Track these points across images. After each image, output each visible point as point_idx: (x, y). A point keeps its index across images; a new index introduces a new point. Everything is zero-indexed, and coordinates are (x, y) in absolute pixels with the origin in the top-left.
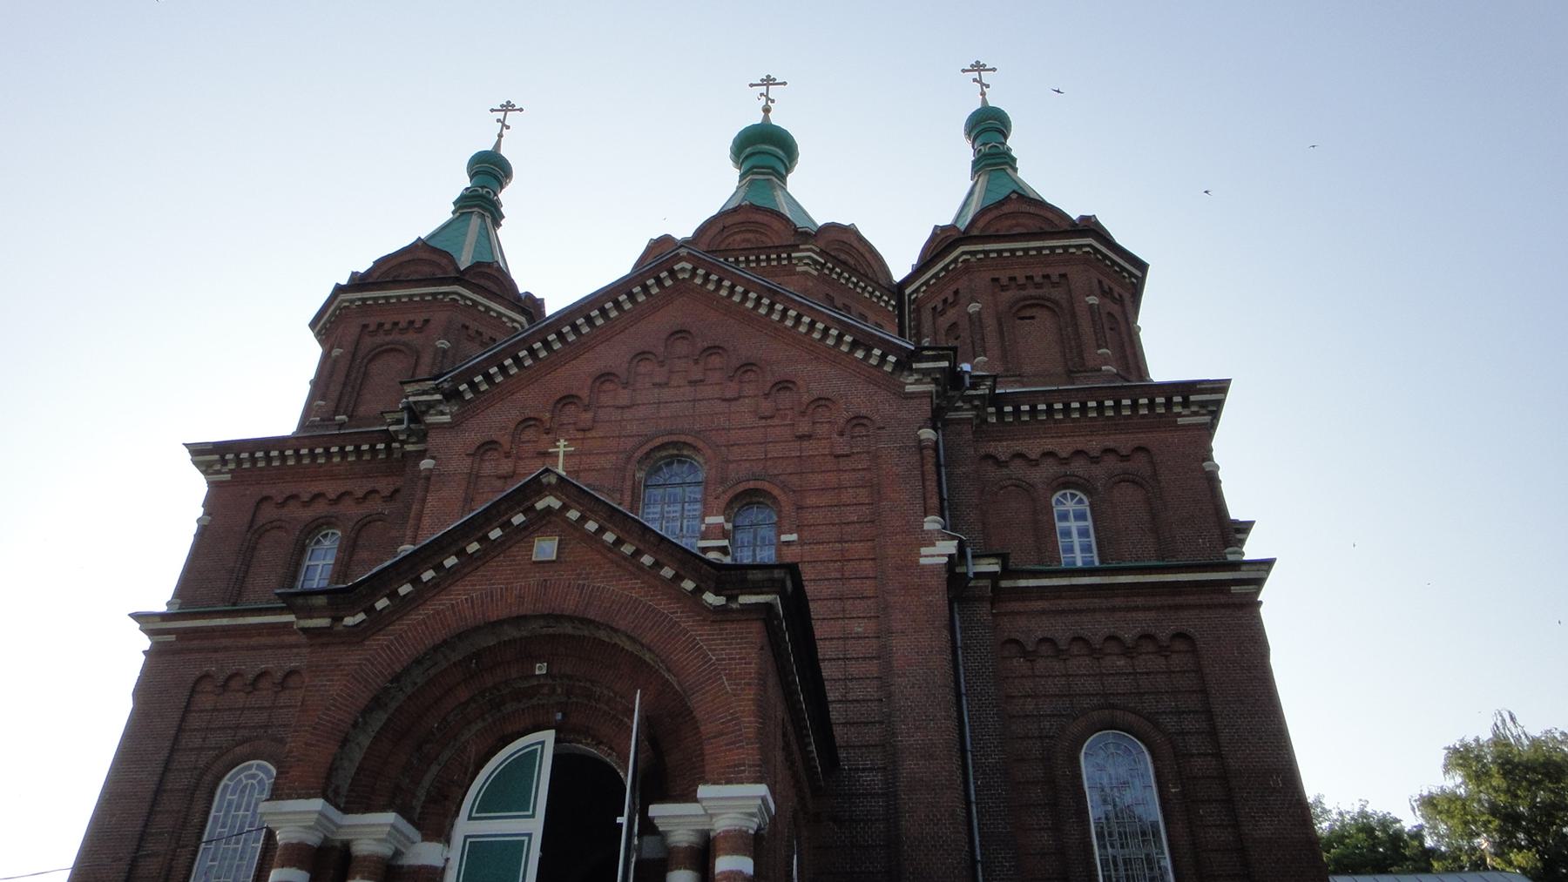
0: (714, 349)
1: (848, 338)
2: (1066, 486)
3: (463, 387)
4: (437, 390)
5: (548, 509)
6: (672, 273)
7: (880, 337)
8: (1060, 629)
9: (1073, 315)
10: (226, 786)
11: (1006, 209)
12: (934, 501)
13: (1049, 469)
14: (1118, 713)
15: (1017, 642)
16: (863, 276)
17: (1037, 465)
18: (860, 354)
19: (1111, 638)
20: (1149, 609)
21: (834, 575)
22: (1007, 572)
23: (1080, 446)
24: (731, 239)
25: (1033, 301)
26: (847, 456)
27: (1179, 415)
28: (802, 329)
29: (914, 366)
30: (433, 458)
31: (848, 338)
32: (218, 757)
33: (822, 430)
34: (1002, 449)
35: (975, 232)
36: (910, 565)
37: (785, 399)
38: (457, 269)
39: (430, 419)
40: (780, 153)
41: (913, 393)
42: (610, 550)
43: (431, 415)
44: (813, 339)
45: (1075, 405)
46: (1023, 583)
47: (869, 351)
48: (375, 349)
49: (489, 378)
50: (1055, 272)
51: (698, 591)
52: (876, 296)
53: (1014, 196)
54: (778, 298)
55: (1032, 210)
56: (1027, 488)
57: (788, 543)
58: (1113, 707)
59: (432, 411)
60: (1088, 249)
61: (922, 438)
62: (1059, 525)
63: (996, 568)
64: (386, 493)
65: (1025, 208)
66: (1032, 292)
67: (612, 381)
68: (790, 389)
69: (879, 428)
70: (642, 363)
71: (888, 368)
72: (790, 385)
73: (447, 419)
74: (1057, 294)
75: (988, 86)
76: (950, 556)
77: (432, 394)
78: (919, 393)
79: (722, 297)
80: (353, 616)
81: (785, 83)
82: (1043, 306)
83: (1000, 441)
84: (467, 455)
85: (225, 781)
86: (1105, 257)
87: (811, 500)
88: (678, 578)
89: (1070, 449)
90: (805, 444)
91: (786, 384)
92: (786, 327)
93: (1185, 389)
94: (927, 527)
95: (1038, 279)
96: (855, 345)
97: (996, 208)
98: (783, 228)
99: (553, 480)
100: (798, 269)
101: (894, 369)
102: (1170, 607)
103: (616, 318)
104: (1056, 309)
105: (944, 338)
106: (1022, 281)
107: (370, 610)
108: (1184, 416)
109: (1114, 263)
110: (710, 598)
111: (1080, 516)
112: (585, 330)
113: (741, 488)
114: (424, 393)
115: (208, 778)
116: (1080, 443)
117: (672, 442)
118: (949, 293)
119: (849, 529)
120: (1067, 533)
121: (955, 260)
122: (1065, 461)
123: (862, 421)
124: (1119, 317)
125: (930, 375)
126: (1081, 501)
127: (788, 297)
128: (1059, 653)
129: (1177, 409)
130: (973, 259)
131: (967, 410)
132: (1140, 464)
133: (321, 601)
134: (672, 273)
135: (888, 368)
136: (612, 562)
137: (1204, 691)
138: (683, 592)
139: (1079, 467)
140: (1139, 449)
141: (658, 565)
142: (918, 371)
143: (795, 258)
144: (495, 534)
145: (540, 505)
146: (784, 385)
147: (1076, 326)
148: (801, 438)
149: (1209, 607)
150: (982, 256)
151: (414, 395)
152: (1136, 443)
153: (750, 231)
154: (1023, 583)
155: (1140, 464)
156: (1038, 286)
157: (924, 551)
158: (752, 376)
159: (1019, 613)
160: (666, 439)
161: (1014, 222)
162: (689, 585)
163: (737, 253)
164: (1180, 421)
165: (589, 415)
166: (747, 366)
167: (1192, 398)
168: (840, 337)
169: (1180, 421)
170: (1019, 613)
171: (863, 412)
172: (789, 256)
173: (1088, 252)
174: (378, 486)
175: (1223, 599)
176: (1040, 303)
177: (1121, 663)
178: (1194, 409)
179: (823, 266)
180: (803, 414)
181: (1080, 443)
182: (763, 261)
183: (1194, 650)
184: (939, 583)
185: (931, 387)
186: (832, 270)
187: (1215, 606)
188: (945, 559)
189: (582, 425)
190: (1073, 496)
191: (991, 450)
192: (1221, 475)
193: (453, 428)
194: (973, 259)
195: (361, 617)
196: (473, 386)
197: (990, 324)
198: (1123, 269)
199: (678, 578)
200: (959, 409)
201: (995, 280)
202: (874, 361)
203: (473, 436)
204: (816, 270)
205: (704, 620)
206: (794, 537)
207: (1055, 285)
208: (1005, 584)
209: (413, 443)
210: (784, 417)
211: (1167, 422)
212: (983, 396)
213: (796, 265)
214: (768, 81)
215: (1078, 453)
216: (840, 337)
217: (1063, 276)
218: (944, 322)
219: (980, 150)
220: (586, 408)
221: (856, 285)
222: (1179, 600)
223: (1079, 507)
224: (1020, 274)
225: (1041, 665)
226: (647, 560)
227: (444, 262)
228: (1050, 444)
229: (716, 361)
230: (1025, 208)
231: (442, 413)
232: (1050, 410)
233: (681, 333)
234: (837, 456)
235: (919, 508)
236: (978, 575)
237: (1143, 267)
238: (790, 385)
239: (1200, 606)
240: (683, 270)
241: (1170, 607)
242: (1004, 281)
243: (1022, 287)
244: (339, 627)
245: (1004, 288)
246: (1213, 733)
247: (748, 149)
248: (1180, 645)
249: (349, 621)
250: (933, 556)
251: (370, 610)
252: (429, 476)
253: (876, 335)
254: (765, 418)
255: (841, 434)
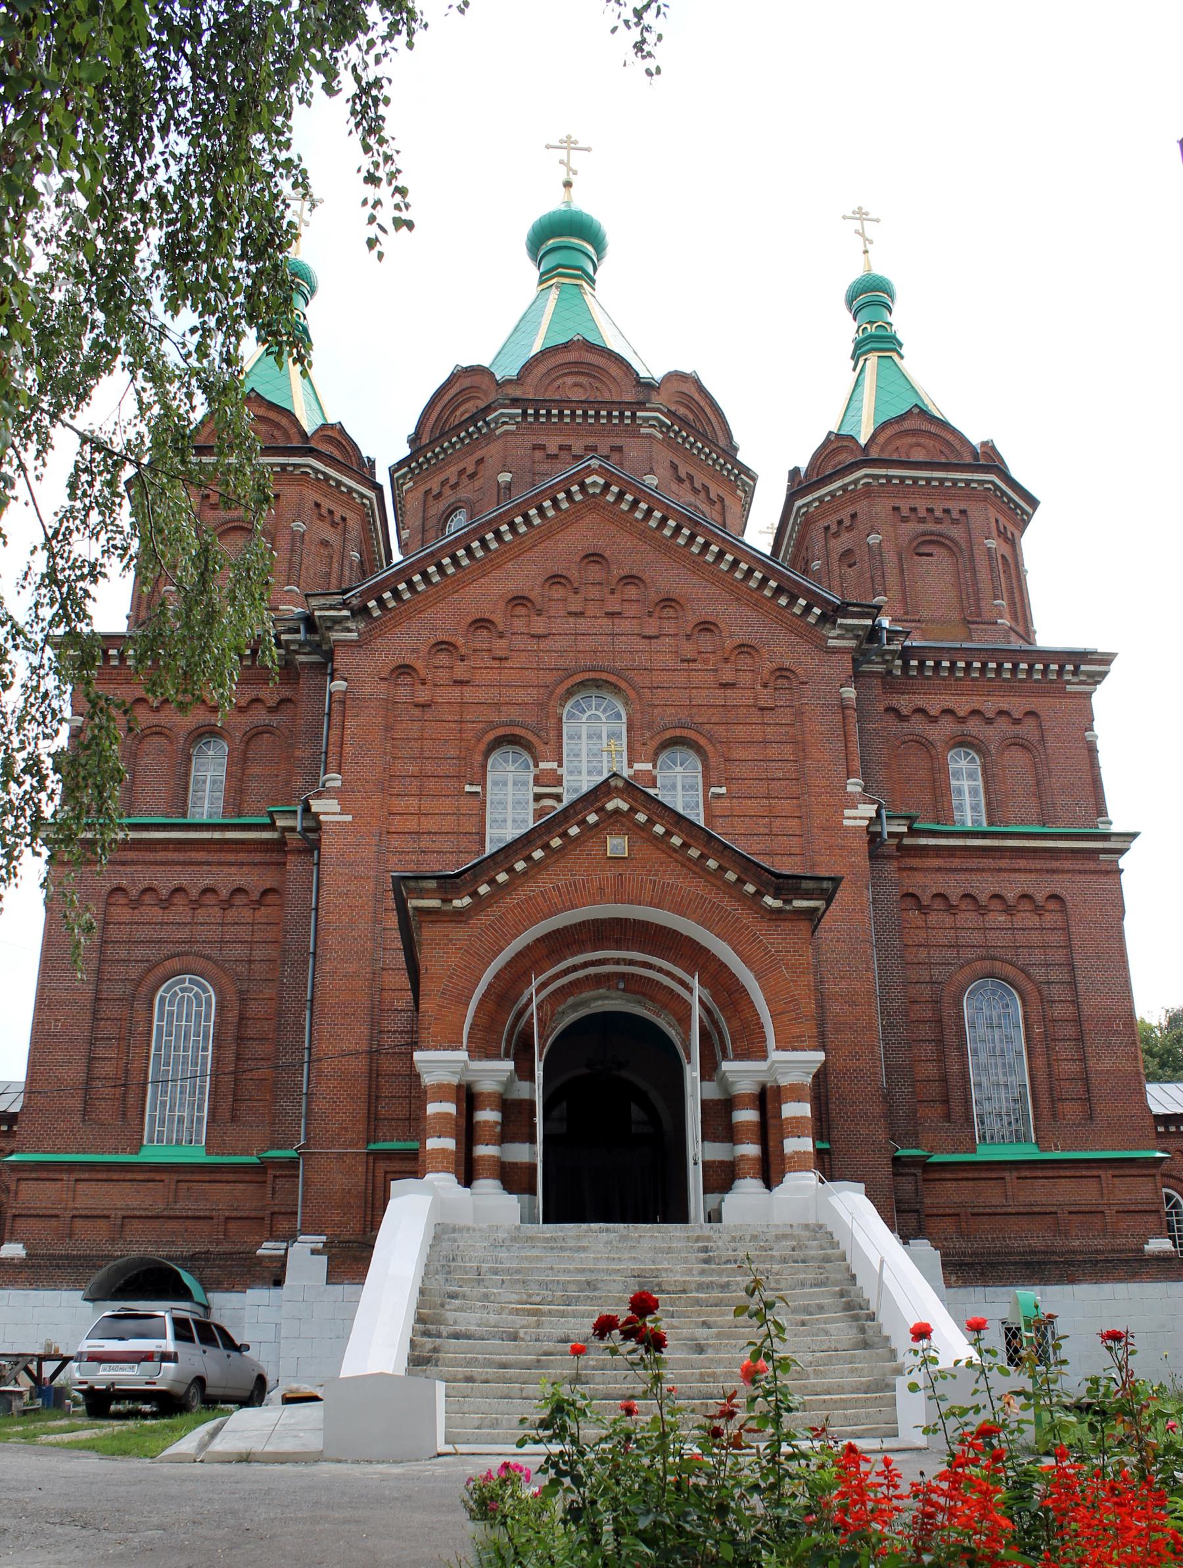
0: (631, 579)
1: (773, 584)
2: (961, 744)
3: (372, 604)
4: (345, 605)
5: (617, 811)
6: (583, 486)
7: (806, 587)
8: (953, 886)
9: (972, 558)
10: (162, 999)
11: (907, 425)
12: (857, 764)
13: (947, 727)
14: (998, 964)
15: (913, 895)
16: (702, 436)
17: (936, 722)
18: (783, 601)
19: (996, 896)
20: (1031, 871)
21: (762, 831)
22: (913, 832)
23: (977, 706)
24: (560, 381)
25: (933, 538)
26: (772, 709)
27: (1069, 682)
28: (724, 567)
29: (839, 621)
30: (345, 680)
31: (773, 584)
32: (149, 970)
33: (745, 678)
34: (904, 703)
35: (874, 454)
36: (834, 827)
37: (706, 641)
38: (303, 434)
39: (335, 635)
40: (590, 249)
41: (835, 647)
42: (675, 851)
43: (337, 631)
44: (736, 579)
45: (977, 665)
46: (923, 841)
47: (793, 600)
48: (227, 523)
49: (396, 594)
50: (955, 507)
51: (759, 894)
52: (682, 437)
53: (916, 411)
54: (699, 530)
55: (933, 429)
56: (924, 744)
57: (719, 796)
58: (994, 958)
59: (337, 627)
60: (989, 486)
61: (844, 696)
62: (954, 783)
63: (905, 829)
64: (271, 703)
65: (925, 426)
66: (931, 526)
67: (525, 606)
68: (711, 631)
69: (802, 683)
70: (554, 587)
71: (811, 620)
72: (712, 627)
73: (354, 636)
74: (955, 532)
75: (871, 242)
76: (871, 819)
77: (340, 610)
78: (840, 648)
79: (636, 520)
80: (461, 899)
81: (588, 150)
82: (943, 544)
83: (903, 693)
84: (381, 679)
85: (160, 992)
86: (1004, 493)
87: (738, 753)
88: (741, 881)
89: (968, 708)
90: (729, 692)
91: (706, 626)
92: (706, 562)
93: (1079, 658)
94: (850, 788)
95: (938, 513)
96: (779, 591)
97: (897, 422)
98: (622, 374)
99: (621, 784)
100: (643, 430)
101: (817, 622)
102: (1048, 871)
103: (525, 534)
104: (955, 549)
105: (836, 564)
106: (922, 513)
107: (474, 894)
108: (1073, 684)
109: (1010, 500)
110: (769, 900)
111: (971, 776)
112: (494, 545)
113: (668, 735)
114: (332, 608)
115: (144, 990)
116: (976, 703)
117: (593, 680)
118: (845, 515)
119: (774, 785)
120: (960, 791)
121: (856, 482)
122: (962, 720)
123: (784, 673)
124: (1010, 560)
125: (852, 631)
126: (973, 760)
127: (711, 531)
128: (951, 909)
129: (1068, 677)
130: (875, 483)
131: (877, 663)
132: (1028, 729)
133: (432, 884)
134: (583, 486)
135: (811, 620)
136: (677, 861)
137: (1069, 946)
138: (727, 883)
139: (974, 727)
140: (1030, 713)
141: (722, 869)
142: (841, 626)
143: (640, 418)
144: (574, 831)
145: (610, 806)
146: (706, 627)
147: (974, 570)
148: (725, 686)
149: (1080, 872)
150: (884, 481)
151: (321, 609)
152: (1028, 708)
153: (583, 374)
154: (923, 841)
155: (1028, 729)
156: (938, 521)
157: (847, 813)
158: (670, 612)
159: (916, 869)
160: (587, 676)
161: (914, 440)
162: (750, 888)
163: (573, 405)
164: (1069, 688)
165: (503, 643)
166: (668, 602)
167: (1083, 668)
168: (764, 581)
169: (1069, 688)
170: (916, 869)
171: (787, 664)
172: (634, 415)
173: (989, 489)
174: (261, 695)
175: (1091, 865)
176: (938, 540)
177: (1002, 919)
178: (1083, 678)
179: (669, 428)
180: (726, 660)
181: (976, 703)
182: (603, 417)
183: (1064, 910)
184: (861, 845)
185: (852, 643)
186: (677, 433)
187: (1085, 872)
188: (867, 822)
189: (499, 654)
190: (967, 754)
191: (894, 704)
192: (1099, 746)
193: (361, 646)
194: (875, 483)
195: (467, 901)
196: (381, 603)
197: (891, 558)
198: (1017, 506)
199: (741, 881)
200: (871, 662)
201: (896, 509)
202: (797, 610)
203: (385, 655)
204: (662, 432)
205: (762, 917)
206: (723, 790)
207: (955, 522)
208: (907, 841)
209: (305, 654)
210: (706, 662)
211: (1056, 688)
212: (895, 651)
213: (640, 426)
214: (569, 144)
215: (975, 712)
216: (764, 581)
217: (963, 512)
218: (839, 545)
219: (865, 328)
220: (501, 636)
221: (700, 450)
222: (1055, 864)
223: (972, 766)
224: (922, 505)
225: (933, 918)
226: (712, 864)
227: (284, 422)
228: (949, 702)
229: (632, 592)
230: (925, 426)
231: (349, 630)
232: (953, 668)
233: (594, 557)
234: (762, 709)
235: (842, 770)
236: (891, 834)
237: (1034, 503)
238: (712, 627)
239: (1074, 871)
240: (594, 484)
241: (1048, 871)
242: (905, 512)
243: (922, 520)
244: (447, 907)
245: (905, 520)
246: (1073, 984)
247: (551, 241)
248: (1052, 905)
249: (457, 903)
250: (855, 818)
251: (474, 894)
252: (343, 699)
253: (801, 585)
254: (688, 661)
255: (765, 686)
